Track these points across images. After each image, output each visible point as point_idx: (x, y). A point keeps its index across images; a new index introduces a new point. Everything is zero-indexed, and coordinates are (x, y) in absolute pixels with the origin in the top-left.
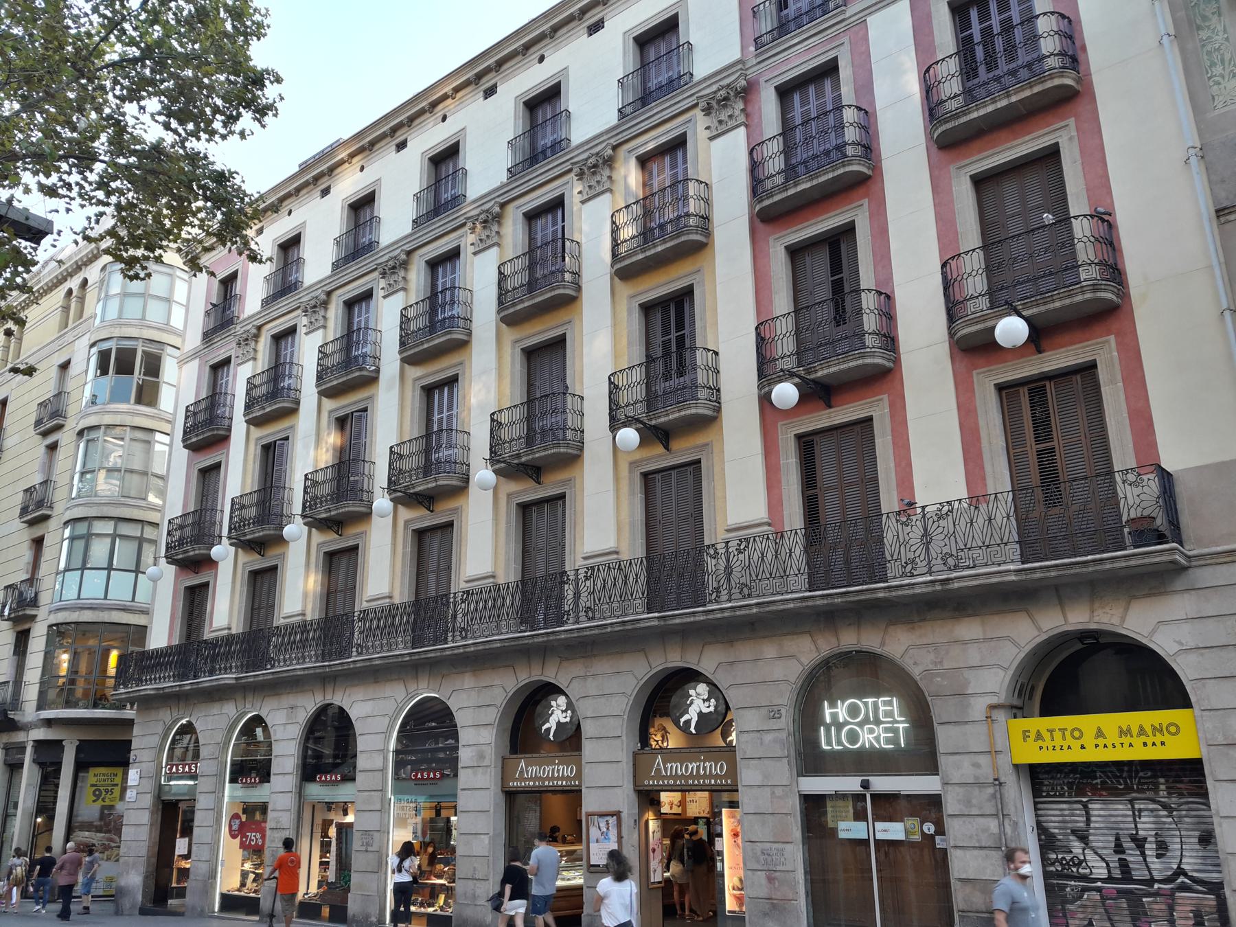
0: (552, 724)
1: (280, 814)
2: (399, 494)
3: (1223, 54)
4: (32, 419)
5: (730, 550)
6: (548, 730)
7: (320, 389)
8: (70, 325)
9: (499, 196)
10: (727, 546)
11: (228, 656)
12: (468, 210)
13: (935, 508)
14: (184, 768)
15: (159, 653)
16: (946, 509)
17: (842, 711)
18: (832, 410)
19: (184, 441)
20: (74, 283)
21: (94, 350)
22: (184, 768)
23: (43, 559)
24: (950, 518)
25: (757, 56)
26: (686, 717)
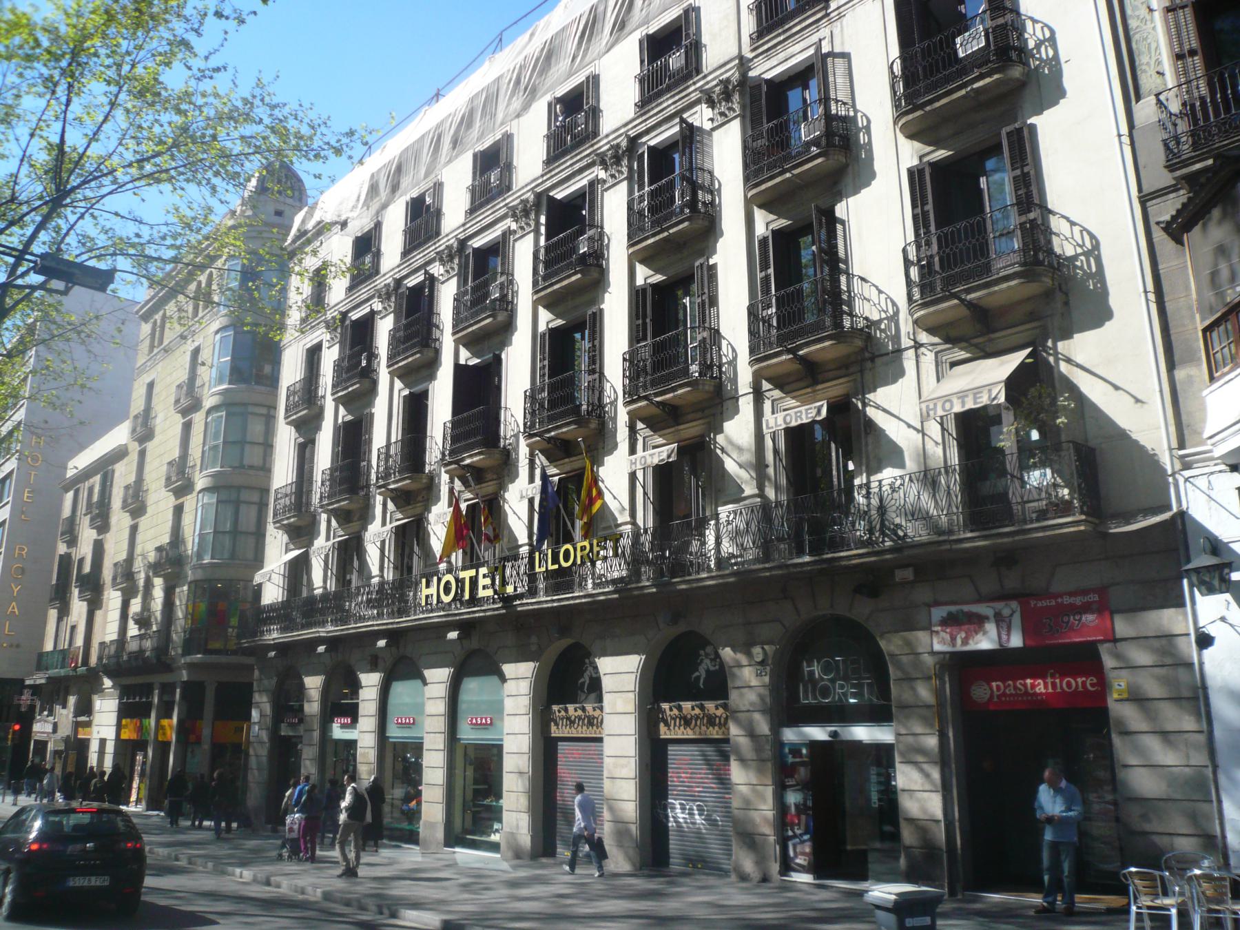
0: (701, 672)
1: (367, 750)
2: (453, 466)
3: (1149, 44)
4: (172, 399)
5: (884, 489)
6: (698, 678)
7: (391, 369)
8: (200, 314)
9: (632, 128)
10: (880, 484)
11: (323, 612)
12: (603, 145)
13: (889, 481)
14: (481, 719)
15: (272, 608)
16: (899, 482)
17: (816, 669)
18: (483, 485)
19: (286, 418)
20: (158, 317)
21: (218, 337)
22: (481, 719)
23: (170, 524)
24: (901, 492)
25: (753, 50)
26: (697, 674)
